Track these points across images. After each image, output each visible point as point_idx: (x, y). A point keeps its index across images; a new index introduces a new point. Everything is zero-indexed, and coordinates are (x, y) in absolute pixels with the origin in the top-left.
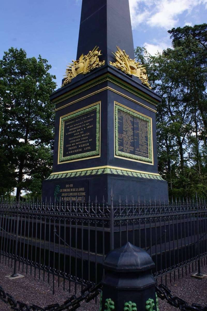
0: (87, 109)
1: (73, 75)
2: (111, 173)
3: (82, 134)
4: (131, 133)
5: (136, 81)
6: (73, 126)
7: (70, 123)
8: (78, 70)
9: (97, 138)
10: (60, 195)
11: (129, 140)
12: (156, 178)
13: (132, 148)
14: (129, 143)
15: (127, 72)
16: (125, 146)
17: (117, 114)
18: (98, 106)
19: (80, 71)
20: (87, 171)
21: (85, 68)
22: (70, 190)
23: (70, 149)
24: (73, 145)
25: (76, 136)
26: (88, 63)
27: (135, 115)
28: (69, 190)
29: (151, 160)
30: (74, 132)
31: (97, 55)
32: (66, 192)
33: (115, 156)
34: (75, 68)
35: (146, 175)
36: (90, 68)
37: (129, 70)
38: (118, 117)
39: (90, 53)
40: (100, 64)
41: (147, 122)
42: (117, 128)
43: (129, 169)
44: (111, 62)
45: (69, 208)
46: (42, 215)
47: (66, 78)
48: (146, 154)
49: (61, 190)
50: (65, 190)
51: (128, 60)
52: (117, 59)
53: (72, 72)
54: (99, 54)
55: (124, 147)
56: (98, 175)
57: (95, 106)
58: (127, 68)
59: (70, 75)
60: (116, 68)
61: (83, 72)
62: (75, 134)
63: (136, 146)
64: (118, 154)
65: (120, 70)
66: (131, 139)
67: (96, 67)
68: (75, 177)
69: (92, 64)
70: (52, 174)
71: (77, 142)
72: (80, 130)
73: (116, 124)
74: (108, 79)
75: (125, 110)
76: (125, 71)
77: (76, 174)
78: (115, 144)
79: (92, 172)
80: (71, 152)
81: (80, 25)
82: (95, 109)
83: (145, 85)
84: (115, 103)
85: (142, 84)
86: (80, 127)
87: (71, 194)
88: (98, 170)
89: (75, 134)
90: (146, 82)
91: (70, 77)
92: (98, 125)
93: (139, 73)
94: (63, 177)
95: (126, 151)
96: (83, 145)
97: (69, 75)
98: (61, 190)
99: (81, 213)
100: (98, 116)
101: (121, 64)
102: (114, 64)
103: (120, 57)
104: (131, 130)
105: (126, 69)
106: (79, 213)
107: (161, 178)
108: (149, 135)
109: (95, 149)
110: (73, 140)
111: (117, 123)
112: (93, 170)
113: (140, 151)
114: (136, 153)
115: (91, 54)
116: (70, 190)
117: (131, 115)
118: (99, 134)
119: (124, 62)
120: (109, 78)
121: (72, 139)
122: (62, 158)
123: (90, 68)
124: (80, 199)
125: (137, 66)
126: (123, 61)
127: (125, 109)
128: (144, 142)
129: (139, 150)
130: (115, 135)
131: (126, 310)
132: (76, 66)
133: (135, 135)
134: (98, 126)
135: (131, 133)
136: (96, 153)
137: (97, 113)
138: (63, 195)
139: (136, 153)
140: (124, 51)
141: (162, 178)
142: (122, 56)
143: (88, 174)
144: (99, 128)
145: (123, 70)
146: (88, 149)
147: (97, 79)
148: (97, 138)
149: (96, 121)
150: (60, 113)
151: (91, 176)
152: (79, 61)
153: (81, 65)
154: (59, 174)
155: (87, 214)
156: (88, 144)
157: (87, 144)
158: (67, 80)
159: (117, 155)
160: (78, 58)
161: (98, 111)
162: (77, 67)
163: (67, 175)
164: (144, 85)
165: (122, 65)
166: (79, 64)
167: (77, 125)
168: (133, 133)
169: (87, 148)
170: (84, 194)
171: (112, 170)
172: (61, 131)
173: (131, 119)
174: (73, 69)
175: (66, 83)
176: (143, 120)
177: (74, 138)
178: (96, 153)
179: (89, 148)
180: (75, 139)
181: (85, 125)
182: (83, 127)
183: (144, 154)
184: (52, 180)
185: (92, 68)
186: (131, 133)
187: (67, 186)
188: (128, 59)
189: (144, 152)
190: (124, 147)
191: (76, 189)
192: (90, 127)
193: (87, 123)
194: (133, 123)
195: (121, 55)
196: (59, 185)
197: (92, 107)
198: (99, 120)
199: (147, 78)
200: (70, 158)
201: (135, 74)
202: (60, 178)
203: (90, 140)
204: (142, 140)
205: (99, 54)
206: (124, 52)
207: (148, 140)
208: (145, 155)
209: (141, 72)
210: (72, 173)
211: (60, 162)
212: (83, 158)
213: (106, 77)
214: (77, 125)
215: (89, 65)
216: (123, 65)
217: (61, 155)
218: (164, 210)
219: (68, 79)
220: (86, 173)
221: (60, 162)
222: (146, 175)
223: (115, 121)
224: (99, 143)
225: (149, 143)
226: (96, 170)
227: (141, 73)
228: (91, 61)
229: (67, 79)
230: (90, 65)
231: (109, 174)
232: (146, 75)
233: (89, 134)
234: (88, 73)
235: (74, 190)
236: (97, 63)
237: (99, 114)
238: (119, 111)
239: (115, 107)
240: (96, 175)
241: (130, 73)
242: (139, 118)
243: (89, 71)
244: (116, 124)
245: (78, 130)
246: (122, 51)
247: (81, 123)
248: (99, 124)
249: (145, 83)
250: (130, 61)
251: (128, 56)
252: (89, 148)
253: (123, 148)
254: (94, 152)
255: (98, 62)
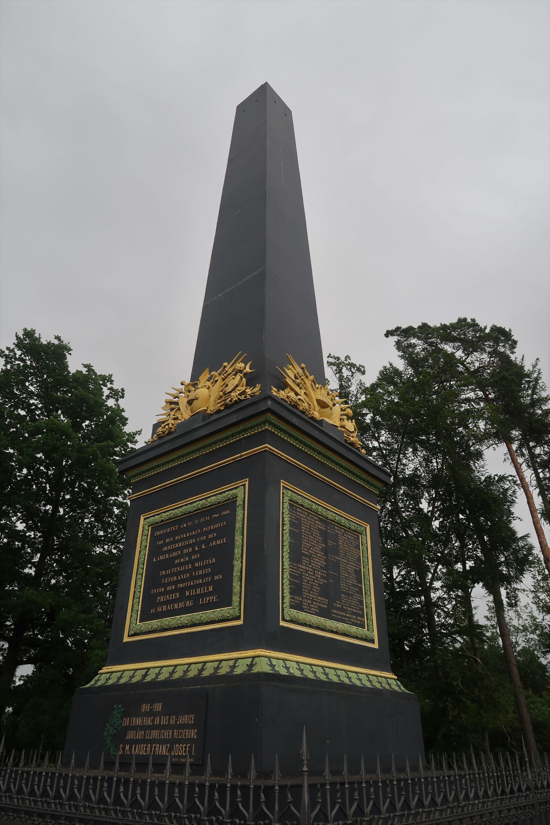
0: (213, 497)
1: (182, 414)
2: (271, 672)
3: (197, 560)
4: (319, 561)
5: (331, 434)
6: (174, 538)
7: (165, 531)
8: (195, 403)
9: (236, 573)
10: (120, 737)
11: (317, 580)
12: (387, 687)
13: (324, 602)
14: (316, 588)
15: (311, 413)
16: (307, 596)
17: (286, 511)
18: (241, 491)
19: (199, 406)
20: (205, 663)
21: (212, 399)
22: (153, 721)
23: (162, 599)
24: (169, 588)
25: (180, 564)
26: (220, 389)
27: (330, 515)
28: (148, 721)
29: (370, 633)
30: (175, 554)
31: (241, 371)
32: (139, 726)
33: (282, 623)
34: (187, 400)
35: (339, 672)
36: (223, 401)
37: (315, 408)
38: (289, 519)
39: (225, 367)
40: (249, 391)
41: (357, 533)
42: (286, 548)
43: (333, 662)
44: (275, 389)
45: (158, 796)
46: (66, 817)
47: (163, 422)
48: (357, 618)
49: (126, 722)
50: (138, 721)
51: (312, 386)
52: (289, 381)
53: (179, 409)
54: (248, 369)
55: (303, 598)
56: (237, 675)
57: (234, 491)
58: (310, 403)
59: (174, 415)
60: (287, 402)
61: (206, 408)
62: (176, 561)
63: (335, 598)
64: (292, 618)
65: (295, 406)
66: (322, 577)
67: (239, 399)
68: (168, 682)
69: (229, 390)
70: (105, 670)
71: (182, 581)
72: (190, 550)
73: (285, 538)
74: (267, 427)
75: (306, 503)
76: (306, 410)
77: (173, 672)
78: (283, 589)
79: (218, 668)
80: (162, 608)
81: (203, 308)
82: (233, 498)
83: (352, 444)
84: (282, 484)
85: (346, 441)
86: (191, 542)
87: (155, 734)
88: (235, 663)
89: (176, 561)
90: (353, 437)
91: (174, 419)
92: (238, 538)
93: (336, 417)
94: (134, 680)
95: (310, 609)
96: (196, 591)
97: (171, 415)
98: (126, 722)
99: (199, 816)
100: (241, 515)
101: (297, 394)
102: (282, 392)
103: (296, 378)
104: (321, 554)
105: (309, 405)
106: (193, 816)
107: (399, 687)
108: (364, 567)
109: (228, 602)
110: (172, 575)
111: (288, 534)
112: (220, 661)
113: (341, 609)
114: (333, 615)
115: (227, 369)
116: (153, 721)
117: (319, 515)
118: (242, 562)
119: (303, 391)
120: (271, 424)
121: (168, 572)
122: (138, 623)
123: (225, 400)
124: (180, 750)
125: (332, 400)
126: (300, 388)
127: (308, 499)
128: (353, 585)
129: (340, 606)
130: (283, 566)
131: (32, 664)
132: (189, 394)
133: (331, 568)
134: (240, 540)
135: (322, 562)
136: (231, 615)
137: (238, 509)
138: (130, 735)
139: (333, 615)
140: (303, 365)
141: (403, 688)
142: (300, 377)
143: (206, 673)
144: (243, 546)
145: (301, 408)
146: (209, 600)
147: (242, 427)
148: (234, 574)
149: (235, 528)
150: (143, 505)
151: (214, 678)
152: (197, 384)
153: (202, 392)
154: (124, 671)
155: (221, 818)
156: (211, 589)
157: (208, 589)
158: (167, 427)
159: (286, 621)
160: (195, 377)
161: (239, 502)
162: (191, 397)
163: (146, 675)
164: (350, 444)
165: (299, 397)
166: (198, 391)
167: (185, 536)
168: (326, 561)
169: (208, 598)
170: (192, 734)
171: (274, 662)
172: (140, 551)
173: (319, 525)
174: (183, 401)
175: (163, 432)
176: (350, 528)
177: (174, 570)
178: (231, 612)
179: (214, 598)
180: (178, 574)
181: (205, 537)
182: (199, 544)
183: (354, 617)
184: (104, 688)
185: (228, 400)
186: (322, 562)
187: (145, 707)
188: (313, 385)
189: (352, 612)
190: (303, 598)
191: (169, 719)
192: (218, 542)
193: (211, 532)
194: (324, 535)
195: (298, 373)
196: (120, 706)
197: (224, 492)
198: (243, 524)
199: (355, 430)
200: (159, 624)
201: (329, 418)
202: (125, 684)
203: (216, 578)
204: (348, 581)
205: (248, 369)
206: (302, 368)
207: (363, 579)
208: (357, 619)
209: (341, 415)
210: (162, 667)
211: (129, 636)
212: (194, 625)
213: (264, 423)
214: (185, 536)
215: (221, 393)
216: (303, 397)
217: (134, 615)
218: (447, 800)
219: (168, 424)
220: (201, 671)
221: (129, 636)
222: (339, 672)
223: (283, 530)
224: (241, 587)
225: (365, 589)
226: (231, 663)
227: (341, 417)
228: (227, 385)
229: (165, 424)
230: (224, 394)
231: (266, 674)
232: (352, 422)
233: (214, 560)
234: (218, 411)
235: (164, 721)
236: (241, 389)
237: (244, 510)
238: (293, 504)
239: (283, 493)
240: (229, 677)
241: (317, 415)
242: (340, 524)
243: (220, 406)
244: (286, 539)
245: (185, 551)
246: (299, 365)
247: (194, 533)
248: (243, 535)
249: (352, 439)
250: (318, 389)
251: (312, 378)
252: (214, 598)
253: (301, 602)
254: (225, 611)
255: (244, 388)
